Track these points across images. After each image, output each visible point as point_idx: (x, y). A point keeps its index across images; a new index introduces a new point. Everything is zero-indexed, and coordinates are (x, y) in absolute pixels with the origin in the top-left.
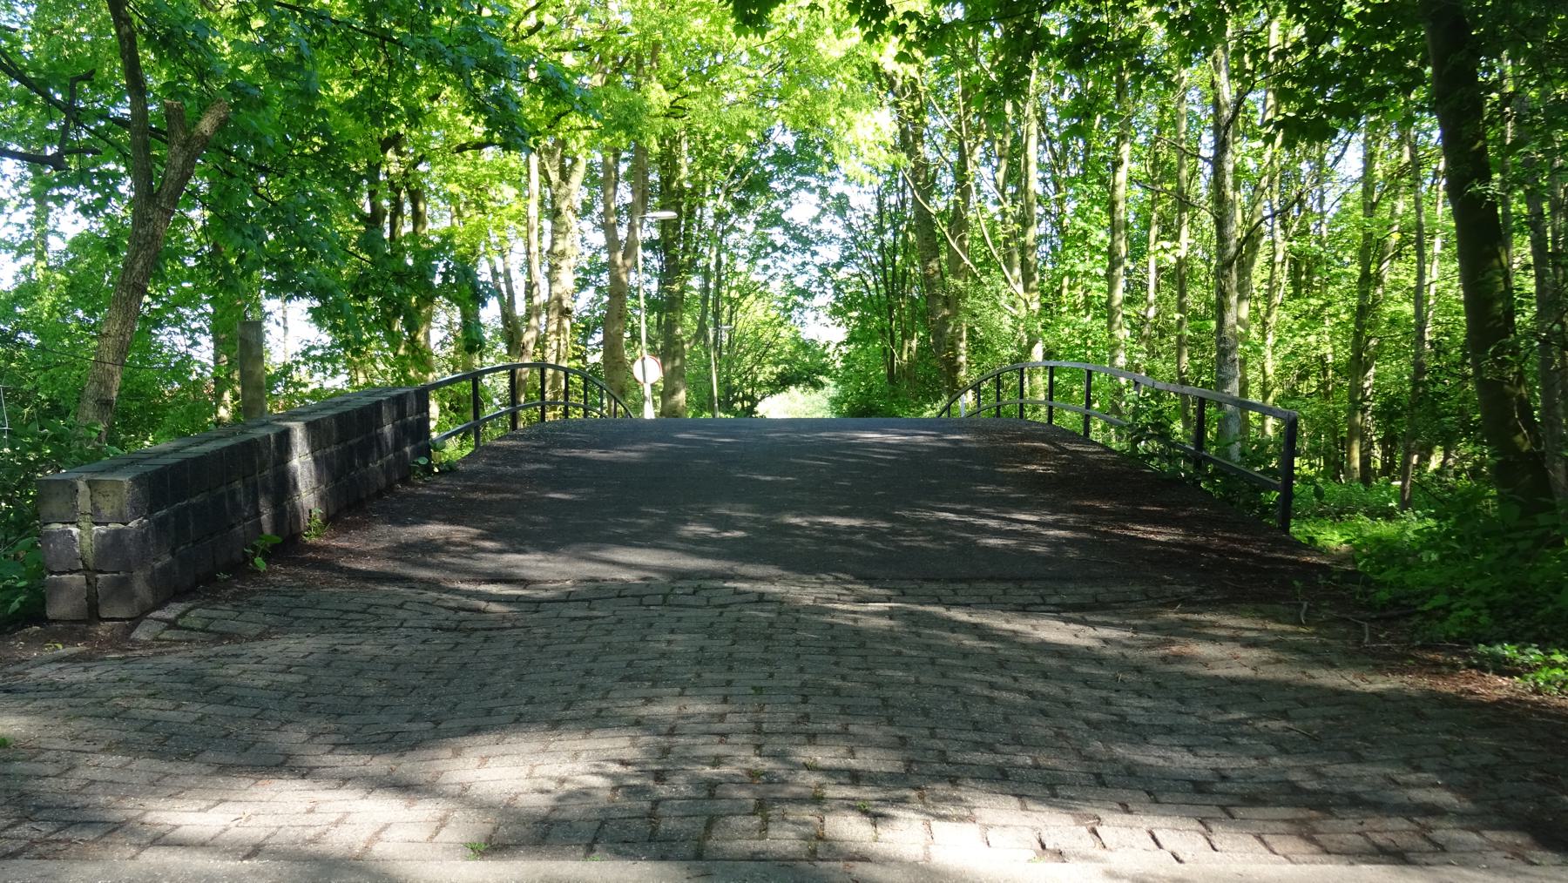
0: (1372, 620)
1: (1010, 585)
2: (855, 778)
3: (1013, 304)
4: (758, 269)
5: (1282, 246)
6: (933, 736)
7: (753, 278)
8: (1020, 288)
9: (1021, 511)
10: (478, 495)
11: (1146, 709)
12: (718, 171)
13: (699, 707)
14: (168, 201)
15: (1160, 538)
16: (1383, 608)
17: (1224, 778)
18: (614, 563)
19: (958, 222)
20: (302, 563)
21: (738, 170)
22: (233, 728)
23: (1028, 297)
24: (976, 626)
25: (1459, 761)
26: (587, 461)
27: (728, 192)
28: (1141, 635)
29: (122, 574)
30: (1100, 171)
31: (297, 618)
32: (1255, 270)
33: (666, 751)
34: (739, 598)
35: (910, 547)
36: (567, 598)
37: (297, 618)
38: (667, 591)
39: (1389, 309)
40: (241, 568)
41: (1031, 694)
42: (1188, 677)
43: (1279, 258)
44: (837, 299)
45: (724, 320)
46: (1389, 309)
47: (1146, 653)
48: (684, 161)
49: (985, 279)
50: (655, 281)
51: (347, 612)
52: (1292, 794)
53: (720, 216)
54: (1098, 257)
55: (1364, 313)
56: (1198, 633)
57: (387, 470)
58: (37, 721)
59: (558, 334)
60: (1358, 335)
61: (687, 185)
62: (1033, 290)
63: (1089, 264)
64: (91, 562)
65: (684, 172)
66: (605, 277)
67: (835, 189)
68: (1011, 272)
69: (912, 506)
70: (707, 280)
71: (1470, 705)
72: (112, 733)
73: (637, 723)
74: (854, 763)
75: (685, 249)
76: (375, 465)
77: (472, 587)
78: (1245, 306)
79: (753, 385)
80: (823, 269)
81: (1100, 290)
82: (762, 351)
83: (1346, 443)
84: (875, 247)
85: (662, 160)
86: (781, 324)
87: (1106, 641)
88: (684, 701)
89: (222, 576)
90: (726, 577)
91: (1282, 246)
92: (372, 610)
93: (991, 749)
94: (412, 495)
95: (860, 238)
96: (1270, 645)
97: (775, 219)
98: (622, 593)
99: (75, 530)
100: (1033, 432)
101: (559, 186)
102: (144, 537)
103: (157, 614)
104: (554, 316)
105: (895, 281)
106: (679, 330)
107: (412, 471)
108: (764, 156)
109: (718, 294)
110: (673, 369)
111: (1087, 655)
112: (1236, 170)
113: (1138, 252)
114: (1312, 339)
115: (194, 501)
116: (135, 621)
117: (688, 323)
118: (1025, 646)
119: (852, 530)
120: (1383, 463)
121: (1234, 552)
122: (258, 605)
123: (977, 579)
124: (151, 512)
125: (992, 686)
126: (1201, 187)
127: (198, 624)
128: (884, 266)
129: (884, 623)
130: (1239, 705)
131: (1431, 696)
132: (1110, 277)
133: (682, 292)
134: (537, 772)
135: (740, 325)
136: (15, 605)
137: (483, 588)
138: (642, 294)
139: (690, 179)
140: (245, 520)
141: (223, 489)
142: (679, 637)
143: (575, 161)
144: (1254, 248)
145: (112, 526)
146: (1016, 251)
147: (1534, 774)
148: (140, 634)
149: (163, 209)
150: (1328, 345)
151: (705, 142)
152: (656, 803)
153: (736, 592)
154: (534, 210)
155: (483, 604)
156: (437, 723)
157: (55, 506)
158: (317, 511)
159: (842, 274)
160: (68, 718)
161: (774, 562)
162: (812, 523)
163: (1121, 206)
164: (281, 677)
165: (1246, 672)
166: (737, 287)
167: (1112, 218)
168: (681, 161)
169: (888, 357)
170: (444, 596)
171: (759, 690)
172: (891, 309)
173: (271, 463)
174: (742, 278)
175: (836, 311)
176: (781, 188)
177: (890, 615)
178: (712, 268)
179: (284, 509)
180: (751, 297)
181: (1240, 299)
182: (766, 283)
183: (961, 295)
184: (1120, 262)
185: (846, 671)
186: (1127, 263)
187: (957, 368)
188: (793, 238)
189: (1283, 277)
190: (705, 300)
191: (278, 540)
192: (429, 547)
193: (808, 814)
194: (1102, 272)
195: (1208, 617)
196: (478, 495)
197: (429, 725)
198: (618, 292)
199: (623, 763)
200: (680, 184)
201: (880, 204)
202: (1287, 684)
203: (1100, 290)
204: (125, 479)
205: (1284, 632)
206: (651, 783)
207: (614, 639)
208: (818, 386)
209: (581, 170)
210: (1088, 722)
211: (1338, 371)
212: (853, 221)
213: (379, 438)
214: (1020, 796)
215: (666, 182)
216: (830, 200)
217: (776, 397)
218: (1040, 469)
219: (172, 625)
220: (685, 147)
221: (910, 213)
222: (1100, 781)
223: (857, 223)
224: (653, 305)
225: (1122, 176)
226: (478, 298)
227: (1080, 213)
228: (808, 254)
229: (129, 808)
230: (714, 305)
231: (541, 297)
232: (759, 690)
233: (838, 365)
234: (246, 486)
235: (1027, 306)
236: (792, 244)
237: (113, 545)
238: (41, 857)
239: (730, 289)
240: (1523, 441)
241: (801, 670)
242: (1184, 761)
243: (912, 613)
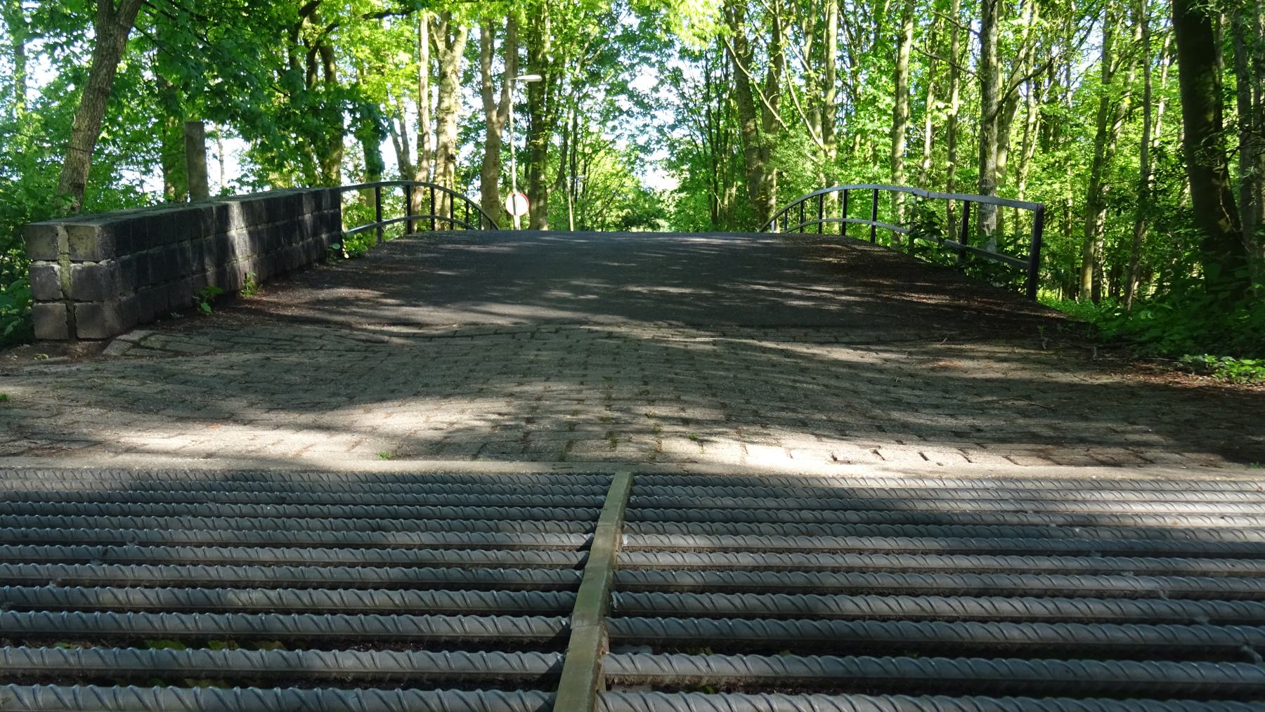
1: (810, 330)
2: (686, 422)
3: (814, 153)
4: (607, 130)
5: (1034, 110)
6: (748, 402)
7: (604, 137)
8: (820, 141)
9: (819, 285)
12: (575, 46)
13: (563, 387)
14: (125, 20)
16: (1108, 341)
17: (979, 430)
18: (491, 313)
19: (771, 85)
20: (240, 311)
21: (591, 45)
22: (188, 397)
25: (1166, 419)
26: (468, 252)
27: (583, 65)
29: (95, 303)
30: (888, 48)
32: (1013, 132)
33: (534, 409)
35: (730, 306)
36: (454, 335)
39: (1120, 162)
40: (191, 311)
43: (1032, 119)
44: (672, 154)
45: (580, 171)
46: (1120, 162)
47: (918, 367)
48: (548, 39)
49: (792, 132)
50: (524, 140)
52: (1034, 438)
54: (885, 118)
55: (1100, 163)
56: (961, 355)
57: (307, 249)
58: (30, 389)
59: (444, 176)
60: (1094, 181)
61: (551, 60)
62: (832, 142)
63: (877, 123)
64: (70, 292)
65: (548, 45)
66: (482, 133)
67: (673, 62)
68: (814, 128)
70: (566, 138)
71: (1175, 389)
72: (92, 397)
73: (511, 395)
74: (683, 415)
75: (548, 111)
76: (298, 245)
77: (378, 328)
78: (1003, 156)
80: (660, 129)
81: (884, 144)
82: (609, 196)
83: (1081, 272)
84: (703, 112)
85: (529, 36)
86: (625, 175)
87: (886, 360)
88: (548, 384)
91: (1034, 110)
93: (794, 411)
94: (328, 271)
95: (691, 105)
96: (1017, 360)
97: (623, 88)
98: (498, 331)
99: (56, 267)
100: (831, 239)
101: (445, 53)
102: (112, 274)
103: (124, 337)
104: (441, 161)
105: (719, 142)
106: (543, 177)
108: (613, 35)
109: (575, 151)
110: (538, 208)
111: (871, 367)
112: (999, 43)
113: (918, 112)
114: (1057, 186)
115: (151, 251)
116: (106, 341)
117: (549, 173)
118: (822, 362)
120: (1110, 292)
121: (990, 311)
122: (206, 334)
123: (783, 326)
124: (118, 256)
125: (795, 381)
126: (971, 64)
127: (157, 345)
128: (710, 128)
130: (991, 393)
131: (1146, 386)
133: (545, 146)
134: (432, 419)
135: (592, 176)
136: (10, 328)
137: (386, 328)
138: (513, 150)
139: (551, 54)
140: (194, 273)
141: (175, 246)
143: (458, 33)
144: (1012, 108)
145: (86, 264)
146: (820, 113)
147: (1225, 424)
148: (112, 350)
149: (121, 26)
150: (1068, 191)
151: (564, 22)
152: (527, 434)
153: (590, 331)
154: (424, 73)
155: (386, 338)
158: (251, 274)
159: (677, 134)
161: (621, 314)
163: (905, 75)
164: (225, 372)
165: (999, 375)
166: (591, 145)
167: (897, 86)
168: (545, 38)
169: (712, 203)
171: (608, 379)
172: (715, 163)
173: (213, 231)
174: (594, 137)
176: (627, 63)
177: (714, 343)
178: (570, 128)
179: (225, 270)
180: (602, 153)
181: (1000, 148)
182: (613, 142)
183: (773, 146)
184: (903, 122)
187: (769, 209)
188: (637, 103)
189: (1034, 137)
190: (564, 154)
191: (220, 291)
192: (343, 302)
193: (649, 439)
194: (887, 130)
195: (968, 346)
198: (494, 145)
199: (500, 414)
200: (544, 56)
201: (708, 77)
202: (1031, 381)
203: (884, 144)
204: (97, 227)
206: (523, 423)
207: (492, 354)
209: (463, 40)
211: (1076, 214)
212: (686, 90)
213: (301, 224)
214: (817, 435)
215: (533, 55)
216: (667, 73)
218: (835, 261)
219: (136, 345)
220: (548, 25)
221: (733, 85)
222: (880, 429)
223: (688, 92)
224: (522, 157)
225: (906, 50)
226: (379, 133)
227: (871, 82)
229: (108, 435)
230: (571, 159)
231: (431, 145)
232: (608, 379)
233: (672, 209)
235: (826, 155)
236: (636, 109)
237: (87, 277)
238: (37, 455)
239: (585, 146)
240: (1225, 224)
242: (945, 421)
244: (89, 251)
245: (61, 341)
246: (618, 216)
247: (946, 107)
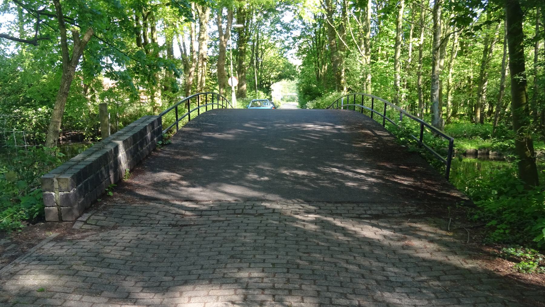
0: (471, 228)
1: (355, 205)
7: (270, 42)
9: (360, 168)
10: (179, 157)
11: (395, 273)
15: (406, 183)
18: (226, 193)
23: (366, 57)
24: (343, 229)
28: (397, 234)
29: (69, 207)
31: (125, 219)
34: (267, 211)
37: (125, 219)
38: (243, 207)
40: (104, 196)
41: (359, 266)
42: (410, 257)
49: (351, 51)
51: (140, 216)
53: (259, 21)
54: (392, 40)
55: (485, 63)
57: (148, 149)
62: (368, 55)
63: (388, 43)
64: (59, 203)
69: (324, 165)
79: (269, 78)
80: (294, 39)
86: (280, 58)
87: (385, 236)
89: (99, 200)
90: (263, 200)
92: (148, 215)
97: (278, 21)
99: (53, 194)
101: (202, 14)
103: (80, 219)
105: (319, 44)
107: (157, 146)
116: (74, 222)
119: (304, 177)
121: (430, 191)
124: (77, 186)
129: (313, 227)
132: (395, 48)
141: (98, 171)
142: (248, 234)
145: (65, 192)
155: (183, 212)
156: (174, 277)
157: (47, 186)
160: (61, 275)
162: (291, 173)
167: (397, 27)
170: (171, 208)
172: (318, 54)
174: (266, 42)
175: (298, 55)
180: (269, 49)
185: (301, 254)
186: (402, 43)
187: (341, 79)
192: (165, 184)
194: (393, 46)
196: (179, 157)
197: (171, 278)
198: (222, 50)
203: (392, 52)
205: (442, 236)
208: (292, 79)
210: (377, 281)
217: (278, 83)
224: (235, 52)
228: (289, 33)
234: (105, 168)
236: (284, 30)
239: (262, 46)
241: (287, 254)
243: (322, 221)
244: (66, 188)
245: (56, 222)
246: (276, 74)
247: (419, 40)
